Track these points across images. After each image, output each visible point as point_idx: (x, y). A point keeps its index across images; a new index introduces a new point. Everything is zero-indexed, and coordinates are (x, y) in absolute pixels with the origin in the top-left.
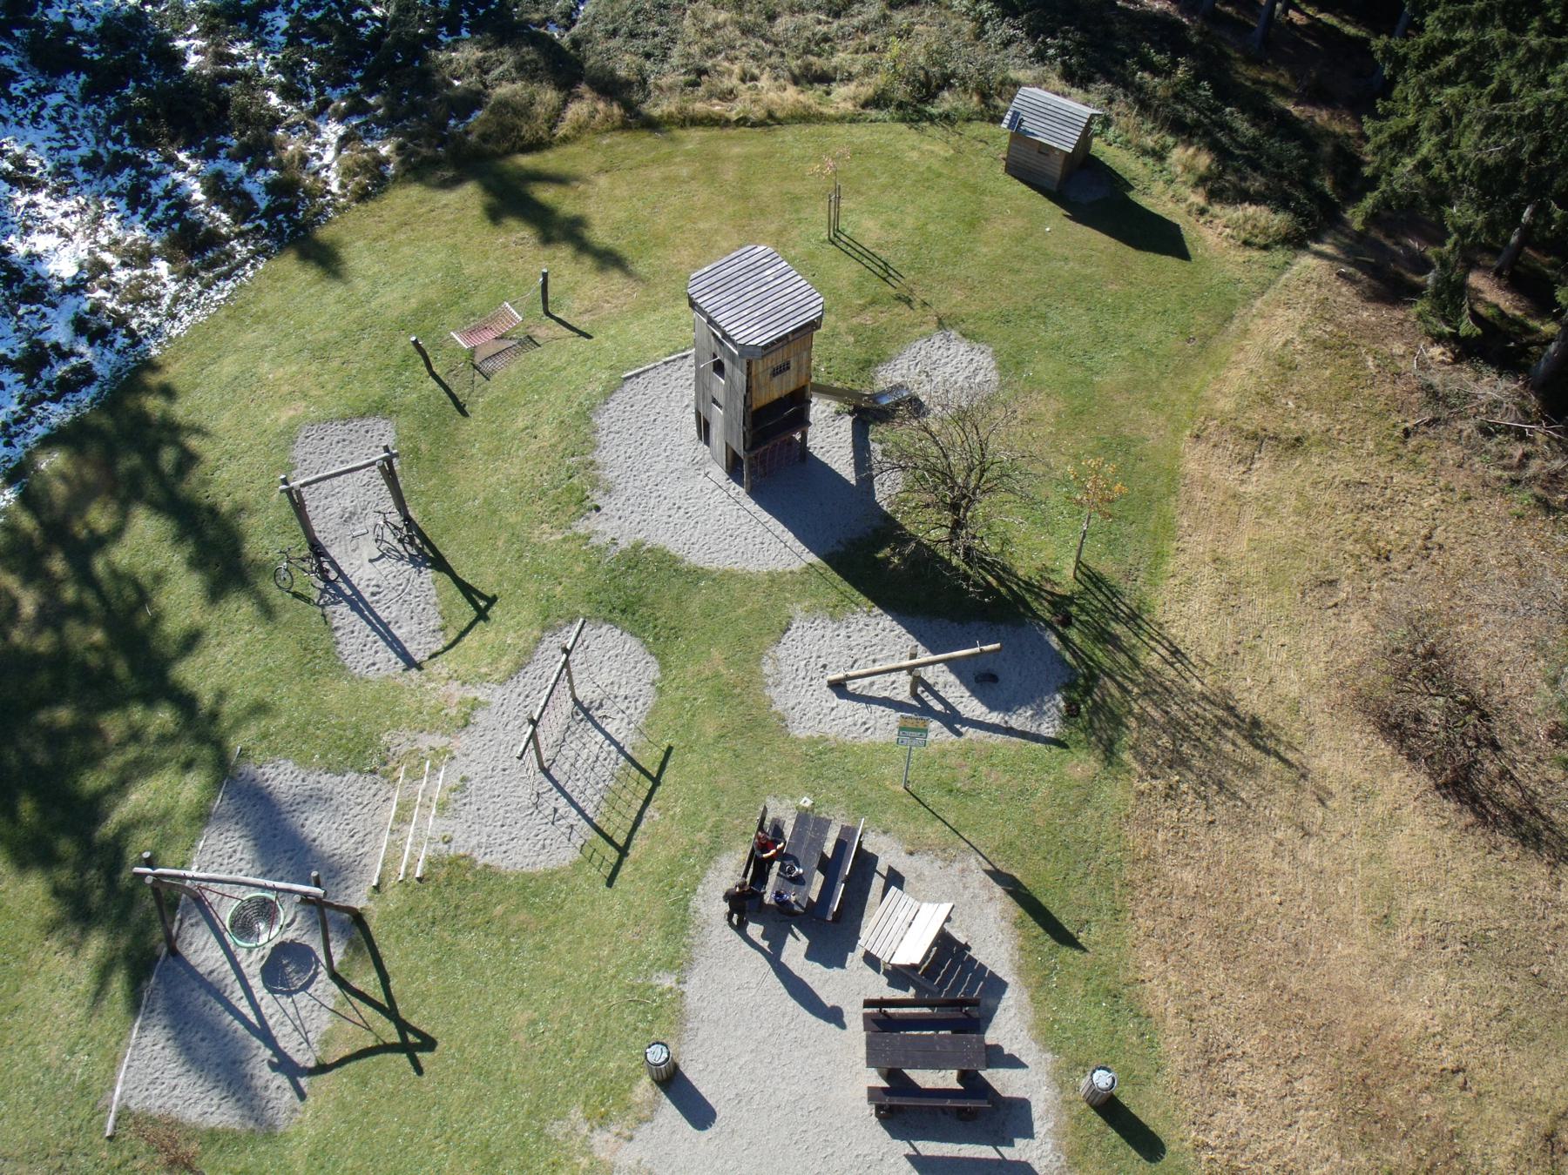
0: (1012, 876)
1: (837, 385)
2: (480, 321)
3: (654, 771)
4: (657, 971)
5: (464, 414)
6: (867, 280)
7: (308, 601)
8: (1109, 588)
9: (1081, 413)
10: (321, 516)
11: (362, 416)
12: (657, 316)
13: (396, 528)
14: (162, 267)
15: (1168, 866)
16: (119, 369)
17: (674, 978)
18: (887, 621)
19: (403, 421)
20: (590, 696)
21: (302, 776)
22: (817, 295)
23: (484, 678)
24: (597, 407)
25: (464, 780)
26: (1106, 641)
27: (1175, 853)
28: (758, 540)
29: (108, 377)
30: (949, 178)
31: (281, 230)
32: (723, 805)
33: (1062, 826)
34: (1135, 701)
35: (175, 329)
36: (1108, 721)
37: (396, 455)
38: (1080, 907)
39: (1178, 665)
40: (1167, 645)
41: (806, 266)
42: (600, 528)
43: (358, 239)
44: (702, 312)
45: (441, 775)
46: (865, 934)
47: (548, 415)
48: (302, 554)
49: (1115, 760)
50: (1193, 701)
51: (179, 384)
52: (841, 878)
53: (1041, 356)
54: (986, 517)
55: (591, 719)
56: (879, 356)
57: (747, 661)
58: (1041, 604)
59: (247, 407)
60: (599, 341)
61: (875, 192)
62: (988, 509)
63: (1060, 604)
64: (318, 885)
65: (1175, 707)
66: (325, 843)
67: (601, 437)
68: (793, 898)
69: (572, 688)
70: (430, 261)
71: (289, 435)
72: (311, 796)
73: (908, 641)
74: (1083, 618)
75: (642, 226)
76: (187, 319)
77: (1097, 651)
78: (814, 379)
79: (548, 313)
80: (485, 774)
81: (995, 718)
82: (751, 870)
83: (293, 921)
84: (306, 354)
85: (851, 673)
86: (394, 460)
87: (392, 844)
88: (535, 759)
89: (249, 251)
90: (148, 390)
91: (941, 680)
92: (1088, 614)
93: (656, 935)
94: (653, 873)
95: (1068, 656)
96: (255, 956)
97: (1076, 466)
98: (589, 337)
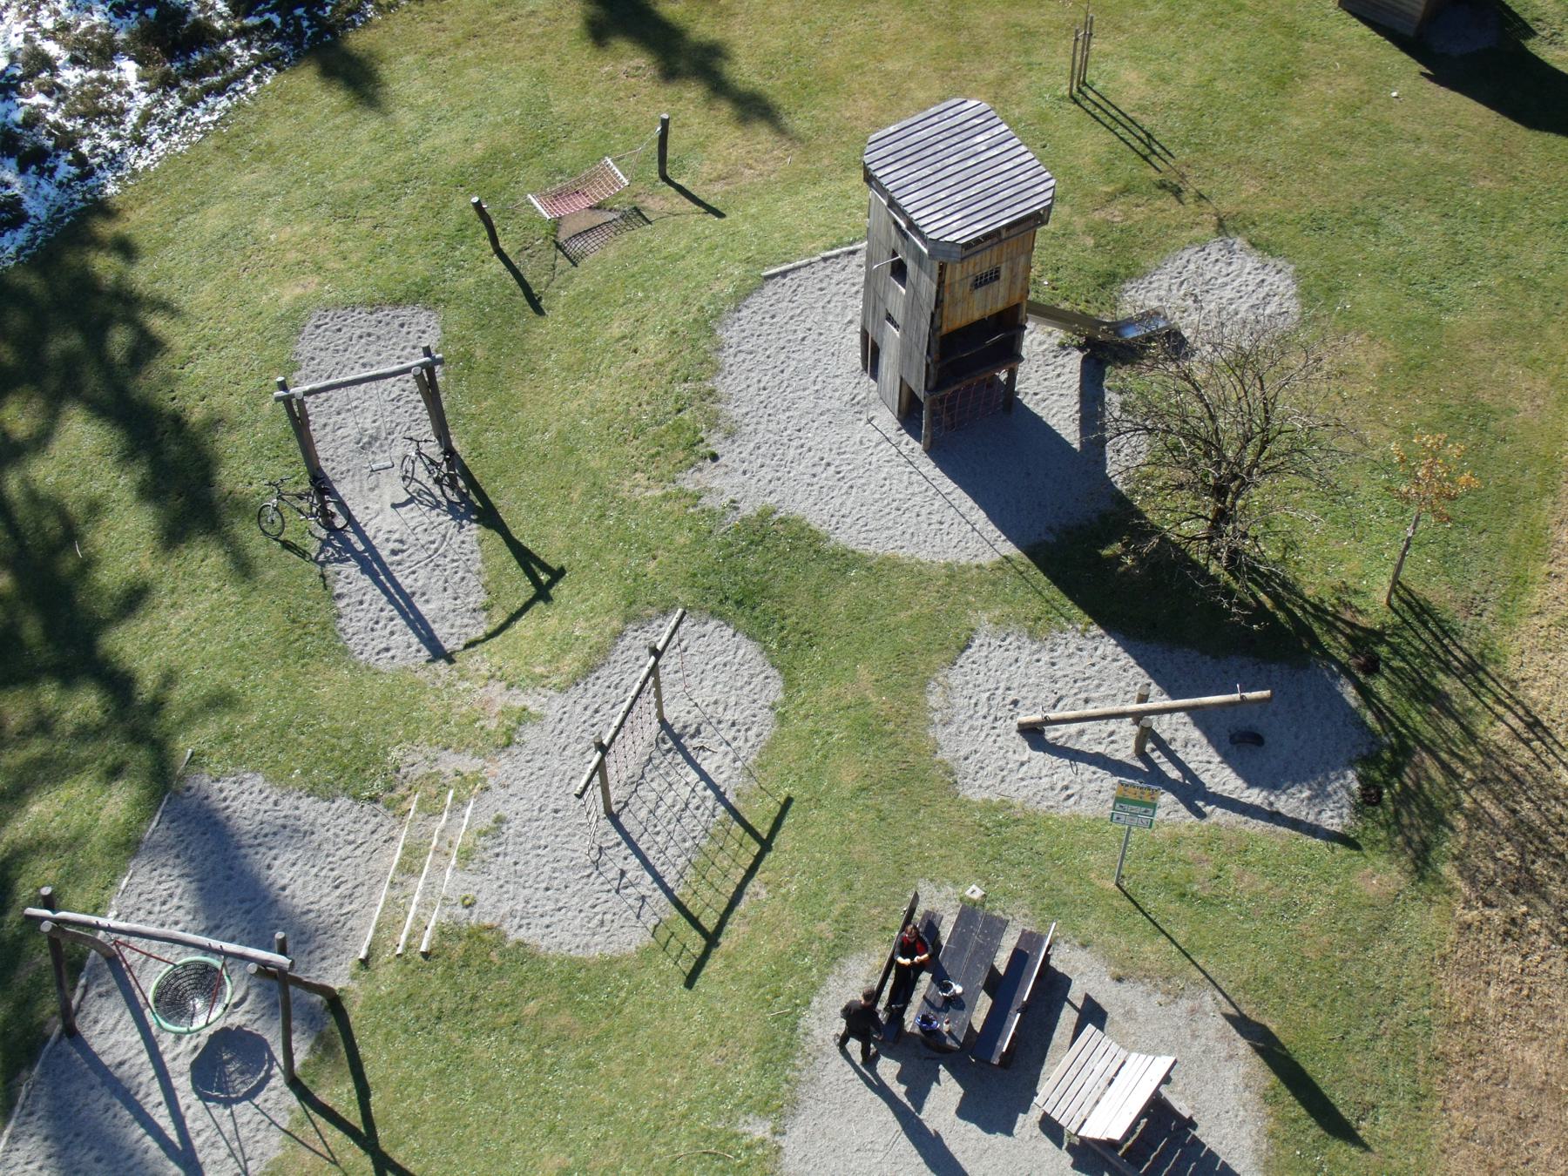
0: (1264, 1028)
1: (1065, 306)
2: (569, 182)
3: (764, 830)
4: (746, 1114)
5: (539, 311)
6: (1120, 158)
7: (303, 554)
8: (1438, 623)
9: (1419, 367)
10: (329, 438)
11: (397, 303)
12: (817, 192)
13: (432, 462)
14: (128, 70)
15: (1502, 1037)
16: (61, 210)
17: (769, 1125)
18: (1109, 646)
19: (453, 314)
20: (684, 718)
21: (274, 797)
22: (1047, 175)
23: (538, 681)
24: (724, 315)
25: (500, 820)
26: (1427, 700)
27: (1514, 1019)
28: (935, 518)
29: (43, 219)
30: (1254, 13)
31: (300, 32)
32: (857, 886)
33: (1344, 961)
34: (1467, 790)
35: (142, 160)
36: (1423, 816)
37: (441, 362)
38: (1364, 1083)
39: (1536, 744)
40: (1521, 712)
41: (1034, 132)
42: (715, 484)
43: (407, 52)
44: (882, 190)
45: (468, 811)
46: (1044, 1089)
47: (654, 321)
48: (300, 489)
49: (1429, 873)
50: (1557, 799)
51: (142, 239)
52: (1015, 1007)
53: (1364, 282)
54: (1265, 509)
55: (682, 749)
56: (1127, 268)
57: (907, 686)
58: (1335, 639)
59: (237, 277)
60: (734, 223)
61: (1143, 29)
62: (1269, 498)
63: (1364, 640)
64: (283, 951)
65: (1527, 805)
66: (298, 893)
67: (727, 358)
68: (946, 1027)
69: (659, 705)
70: (505, 92)
71: (293, 322)
72: (284, 827)
73: (1137, 676)
74: (1396, 663)
75: (805, 61)
76: (160, 146)
77: (1413, 714)
78: (1032, 296)
79: (665, 178)
80: (528, 814)
81: (1255, 796)
82: (890, 982)
83: (243, 1000)
84: (323, 209)
85: (1052, 715)
86: (437, 368)
87: (391, 902)
88: (600, 800)
89: (253, 56)
90: (98, 244)
91: (1181, 735)
92: (1404, 659)
93: (749, 1062)
94: (751, 974)
95: (1369, 718)
96: (185, 1045)
97: (1404, 443)
98: (720, 215)
